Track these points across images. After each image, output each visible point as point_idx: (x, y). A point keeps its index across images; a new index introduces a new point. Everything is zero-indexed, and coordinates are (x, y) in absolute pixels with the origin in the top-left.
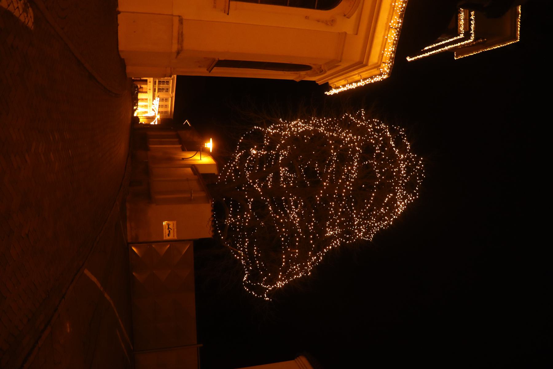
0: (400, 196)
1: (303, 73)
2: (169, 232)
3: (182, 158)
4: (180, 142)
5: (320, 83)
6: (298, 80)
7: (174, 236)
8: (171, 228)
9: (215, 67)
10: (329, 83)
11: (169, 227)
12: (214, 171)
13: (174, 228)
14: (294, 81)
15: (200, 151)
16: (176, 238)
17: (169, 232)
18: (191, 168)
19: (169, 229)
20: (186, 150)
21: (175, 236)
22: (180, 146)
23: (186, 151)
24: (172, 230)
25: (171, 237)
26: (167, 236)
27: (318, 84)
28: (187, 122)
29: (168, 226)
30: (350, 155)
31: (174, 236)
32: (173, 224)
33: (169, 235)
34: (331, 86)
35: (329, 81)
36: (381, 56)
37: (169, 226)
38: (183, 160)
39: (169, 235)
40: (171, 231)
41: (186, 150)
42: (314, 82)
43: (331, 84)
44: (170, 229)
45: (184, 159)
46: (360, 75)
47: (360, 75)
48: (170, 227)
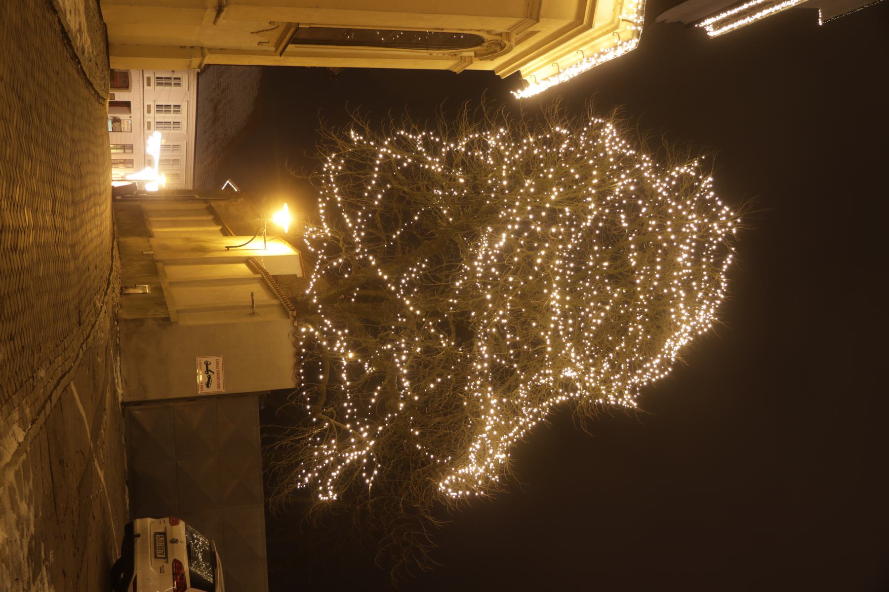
0: (615, 135)
1: (468, 53)
2: (209, 377)
3: (226, 247)
4: (217, 220)
5: (503, 74)
6: (458, 70)
7: (219, 388)
8: (212, 370)
9: (293, 43)
10: (522, 74)
11: (209, 369)
12: (296, 270)
13: (218, 371)
14: (451, 71)
15: (260, 235)
16: (222, 390)
17: (209, 377)
18: (246, 264)
19: (208, 373)
20: (233, 234)
21: (222, 387)
22: (219, 228)
23: (232, 235)
24: (215, 374)
25: (213, 389)
26: (205, 386)
27: (499, 76)
28: (228, 184)
29: (207, 367)
30: (587, 270)
31: (219, 388)
32: (217, 363)
33: (208, 385)
34: (526, 81)
35: (521, 69)
36: (619, 7)
37: (209, 366)
38: (228, 249)
39: (208, 385)
40: (214, 377)
41: (233, 234)
42: (492, 73)
43: (527, 75)
44: (210, 373)
45: (230, 249)
46: (582, 51)
47: (582, 51)
48: (210, 367)
